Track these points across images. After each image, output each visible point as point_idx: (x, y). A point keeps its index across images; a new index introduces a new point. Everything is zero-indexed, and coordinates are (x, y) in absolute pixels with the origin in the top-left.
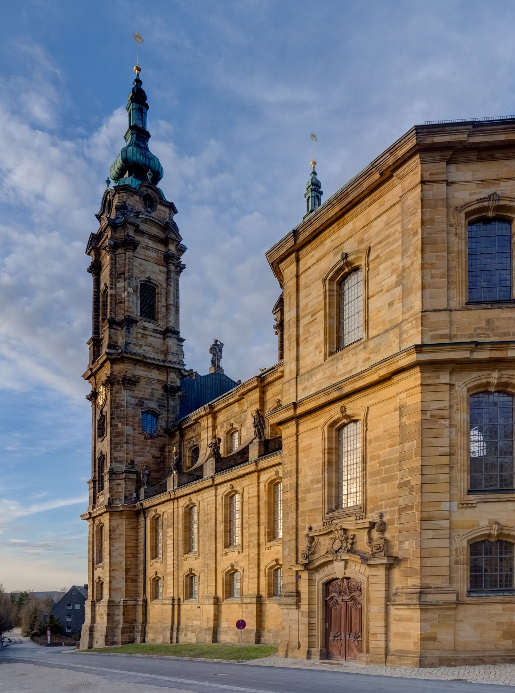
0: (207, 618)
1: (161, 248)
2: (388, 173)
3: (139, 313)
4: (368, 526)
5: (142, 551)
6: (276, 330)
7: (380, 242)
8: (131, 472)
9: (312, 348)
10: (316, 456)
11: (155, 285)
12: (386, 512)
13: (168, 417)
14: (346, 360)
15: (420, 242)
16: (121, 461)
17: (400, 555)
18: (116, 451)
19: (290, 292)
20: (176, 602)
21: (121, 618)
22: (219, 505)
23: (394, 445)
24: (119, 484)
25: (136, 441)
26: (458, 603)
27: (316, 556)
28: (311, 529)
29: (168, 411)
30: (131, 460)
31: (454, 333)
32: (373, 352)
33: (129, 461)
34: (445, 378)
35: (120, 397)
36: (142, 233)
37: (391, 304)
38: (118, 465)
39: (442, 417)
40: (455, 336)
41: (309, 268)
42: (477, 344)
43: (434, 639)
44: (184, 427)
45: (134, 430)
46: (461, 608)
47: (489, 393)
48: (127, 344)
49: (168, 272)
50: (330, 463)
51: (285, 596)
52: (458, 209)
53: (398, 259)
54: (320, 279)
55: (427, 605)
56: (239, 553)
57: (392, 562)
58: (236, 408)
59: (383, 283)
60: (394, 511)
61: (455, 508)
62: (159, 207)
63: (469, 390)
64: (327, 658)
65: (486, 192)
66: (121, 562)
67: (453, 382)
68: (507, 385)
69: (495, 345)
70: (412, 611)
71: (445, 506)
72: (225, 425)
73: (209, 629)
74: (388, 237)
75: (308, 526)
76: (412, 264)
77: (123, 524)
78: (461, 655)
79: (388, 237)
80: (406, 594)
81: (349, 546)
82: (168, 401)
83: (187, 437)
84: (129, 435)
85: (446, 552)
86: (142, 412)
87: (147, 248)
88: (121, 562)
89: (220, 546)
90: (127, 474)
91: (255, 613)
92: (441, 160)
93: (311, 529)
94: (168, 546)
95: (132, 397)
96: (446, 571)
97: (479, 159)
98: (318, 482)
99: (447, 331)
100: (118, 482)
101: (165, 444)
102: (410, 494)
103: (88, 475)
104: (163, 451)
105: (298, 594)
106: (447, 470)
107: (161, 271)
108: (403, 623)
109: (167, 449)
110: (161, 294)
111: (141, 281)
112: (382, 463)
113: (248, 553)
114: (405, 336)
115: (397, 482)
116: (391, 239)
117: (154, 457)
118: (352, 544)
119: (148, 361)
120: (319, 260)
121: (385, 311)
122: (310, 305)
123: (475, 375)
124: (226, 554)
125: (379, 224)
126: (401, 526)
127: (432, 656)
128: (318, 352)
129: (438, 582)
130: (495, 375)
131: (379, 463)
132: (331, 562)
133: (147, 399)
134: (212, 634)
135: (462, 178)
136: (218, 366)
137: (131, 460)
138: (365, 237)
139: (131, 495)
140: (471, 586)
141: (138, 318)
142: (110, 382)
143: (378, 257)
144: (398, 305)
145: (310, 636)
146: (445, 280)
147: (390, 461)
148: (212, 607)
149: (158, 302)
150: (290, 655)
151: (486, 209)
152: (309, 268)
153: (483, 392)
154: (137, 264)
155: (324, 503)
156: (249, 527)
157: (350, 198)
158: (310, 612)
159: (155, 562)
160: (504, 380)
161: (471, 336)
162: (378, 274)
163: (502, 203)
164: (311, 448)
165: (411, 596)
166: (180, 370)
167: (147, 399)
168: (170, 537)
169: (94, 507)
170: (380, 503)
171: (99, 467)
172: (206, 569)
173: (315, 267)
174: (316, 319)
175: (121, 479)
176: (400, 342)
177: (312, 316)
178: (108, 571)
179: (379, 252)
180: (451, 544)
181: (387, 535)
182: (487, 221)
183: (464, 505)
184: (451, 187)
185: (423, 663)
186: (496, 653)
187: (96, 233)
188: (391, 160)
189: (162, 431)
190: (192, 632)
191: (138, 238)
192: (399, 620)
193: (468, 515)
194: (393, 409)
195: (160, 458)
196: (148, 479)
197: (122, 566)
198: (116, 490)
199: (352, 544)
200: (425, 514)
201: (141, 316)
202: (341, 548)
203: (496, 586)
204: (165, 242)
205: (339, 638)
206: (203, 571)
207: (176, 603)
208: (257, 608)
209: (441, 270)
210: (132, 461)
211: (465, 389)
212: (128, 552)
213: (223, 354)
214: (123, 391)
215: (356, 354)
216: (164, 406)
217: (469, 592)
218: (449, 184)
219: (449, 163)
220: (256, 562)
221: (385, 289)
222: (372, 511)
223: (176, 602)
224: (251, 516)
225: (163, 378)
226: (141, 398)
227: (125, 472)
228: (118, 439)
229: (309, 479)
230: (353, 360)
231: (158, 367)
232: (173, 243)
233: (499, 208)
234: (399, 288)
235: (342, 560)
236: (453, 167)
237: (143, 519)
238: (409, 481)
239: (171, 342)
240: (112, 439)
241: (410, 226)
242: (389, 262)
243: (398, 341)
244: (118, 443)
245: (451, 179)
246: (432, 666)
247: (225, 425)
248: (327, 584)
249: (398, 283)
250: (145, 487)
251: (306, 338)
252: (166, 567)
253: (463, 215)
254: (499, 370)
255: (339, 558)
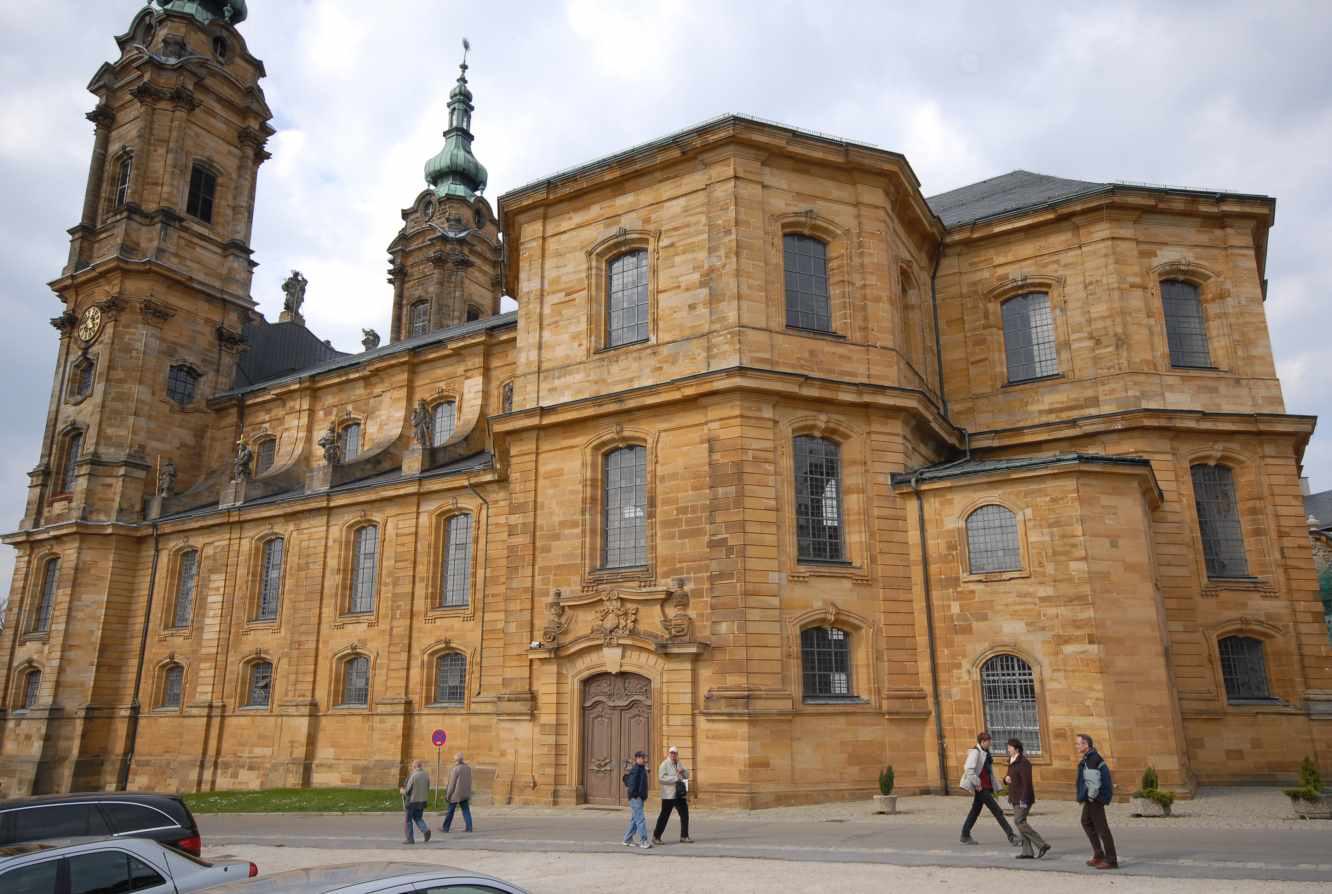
0: (292, 742)
1: (235, 119)
2: (690, 154)
3: (185, 208)
4: (663, 596)
5: (142, 612)
6: (391, 277)
7: (675, 229)
8: (136, 466)
9: (566, 337)
10: (570, 488)
11: (218, 170)
12: (689, 579)
13: (216, 383)
14: (623, 363)
15: (734, 244)
16: (120, 446)
17: (714, 641)
18: (111, 426)
19: (531, 256)
20: (217, 712)
21: (76, 744)
22: (334, 541)
23: (701, 488)
24: (110, 486)
25: (154, 413)
26: (796, 714)
27: (570, 638)
28: (558, 594)
29: (218, 371)
30: (140, 446)
31: (776, 358)
32: (666, 362)
33: (136, 448)
34: (768, 413)
35: (134, 334)
36: (207, 90)
37: (692, 307)
38: (112, 450)
39: (766, 461)
40: (777, 363)
41: (564, 232)
42: (807, 378)
43: (766, 765)
44: (250, 402)
45: (153, 394)
46: (798, 719)
47: (812, 437)
48: (160, 251)
49: (243, 158)
50: (593, 499)
51: (509, 700)
52: (775, 217)
53: (702, 255)
54: (582, 249)
55: (756, 715)
56: (370, 625)
57: (701, 651)
58: (360, 391)
59: (681, 279)
60: (702, 578)
61: (784, 582)
62: (238, 60)
63: (794, 431)
64: (586, 801)
65: (803, 207)
66: (92, 632)
67: (777, 418)
68: (834, 431)
69: (826, 383)
70: (735, 724)
71: (774, 577)
72: (334, 413)
73: (294, 762)
74: (688, 226)
75: (553, 591)
76: (724, 266)
77: (105, 563)
78: (803, 789)
79: (688, 226)
80: (725, 698)
81: (630, 625)
82: (220, 354)
83: (250, 420)
84: (143, 402)
85: (775, 641)
86: (172, 367)
87: (211, 113)
88: (92, 632)
89: (328, 612)
90: (129, 469)
91: (400, 732)
92: (757, 160)
93: (558, 594)
94: (209, 606)
95: (157, 338)
96: (777, 667)
97: (795, 170)
98: (574, 524)
99: (767, 356)
100: (109, 480)
101: (207, 426)
102: (728, 557)
103: (32, 456)
104: (202, 438)
105: (533, 697)
106: (773, 529)
107: (230, 152)
108: (720, 742)
109: (209, 434)
110: (228, 187)
111: (195, 160)
112: (683, 510)
113: (388, 628)
114: (715, 351)
115: (706, 538)
116: (692, 230)
117: (183, 445)
118: (635, 621)
119: (196, 286)
120: (580, 226)
121: (684, 313)
122: (564, 279)
123: (800, 413)
124: (342, 626)
125: (676, 206)
126: (714, 601)
127: (767, 789)
128: (576, 344)
129: (772, 683)
130: (823, 417)
131: (677, 509)
132: (599, 647)
133: (182, 346)
134: (301, 770)
135: (776, 185)
136: (297, 313)
137: (140, 446)
138: (653, 217)
139: (132, 506)
140: (804, 692)
141: (183, 214)
142: (113, 307)
143: (672, 245)
144: (703, 311)
145: (557, 765)
146: (763, 294)
147: (694, 509)
148: (304, 722)
149: (221, 198)
150: (516, 798)
151: (803, 225)
152: (564, 232)
153: (806, 436)
154: (193, 134)
155: (583, 557)
156: (395, 584)
157: (637, 167)
158: (558, 729)
159: (172, 635)
160: (831, 425)
161: (793, 366)
162: (673, 266)
163: (819, 223)
164: (562, 475)
165: (734, 701)
166: (249, 309)
167: (182, 346)
168: (218, 589)
169: (36, 524)
170: (678, 565)
171: (61, 449)
172: (295, 653)
173: (574, 233)
174: (573, 300)
175: (117, 477)
176: (709, 357)
177: (567, 295)
178: (59, 648)
179: (674, 239)
180: (781, 630)
181: (692, 613)
182: (801, 236)
183: (795, 579)
184: (766, 191)
185: (753, 802)
186: (843, 786)
187: (112, 63)
188: (698, 143)
189: (204, 403)
190: (251, 768)
191: (199, 96)
192: (713, 738)
193: (798, 592)
194: (698, 440)
195: (194, 448)
196: (171, 481)
197: (93, 639)
198: (100, 495)
199: (635, 621)
200: (750, 587)
201: (188, 211)
202: (617, 627)
203: (814, 690)
204: (244, 113)
205: (608, 768)
206: (287, 655)
207: (215, 713)
208: (405, 722)
209: (759, 282)
210: (142, 447)
211: (790, 430)
212: (111, 612)
213: (306, 296)
214: (140, 326)
215: (640, 358)
216: (212, 363)
217: (805, 698)
218: (764, 187)
219: (763, 164)
220: (406, 642)
221: (683, 285)
222: (666, 575)
223: (217, 712)
224: (400, 565)
225: (217, 317)
226: (174, 343)
227: (126, 464)
228: (119, 406)
229: (556, 519)
230: (635, 365)
231: (210, 298)
232: (256, 119)
233: (815, 227)
234: (705, 292)
235: (619, 645)
236: (767, 170)
237: (153, 552)
238: (725, 540)
239: (236, 264)
240: (107, 403)
241: (720, 222)
242: (689, 256)
243: (705, 354)
244: (117, 412)
245: (766, 183)
246: (766, 805)
247: (334, 413)
248: (587, 682)
249: (702, 284)
250: (164, 495)
251: (556, 322)
252: (199, 644)
253: (779, 225)
254: (827, 413)
255: (614, 642)
